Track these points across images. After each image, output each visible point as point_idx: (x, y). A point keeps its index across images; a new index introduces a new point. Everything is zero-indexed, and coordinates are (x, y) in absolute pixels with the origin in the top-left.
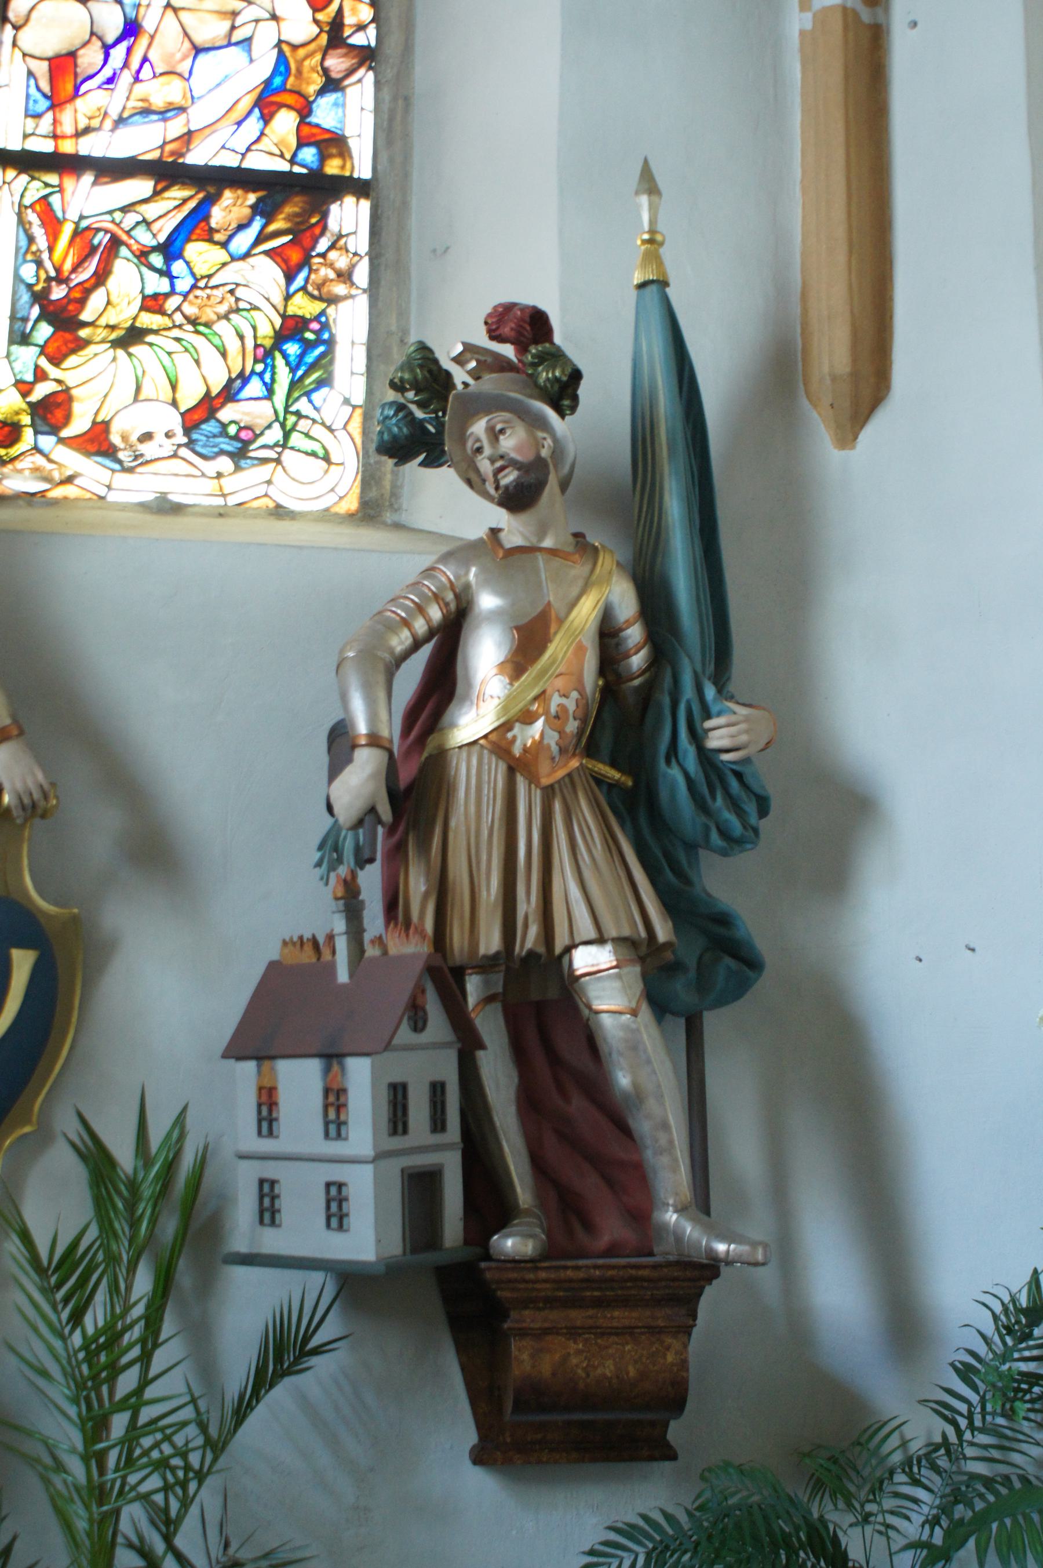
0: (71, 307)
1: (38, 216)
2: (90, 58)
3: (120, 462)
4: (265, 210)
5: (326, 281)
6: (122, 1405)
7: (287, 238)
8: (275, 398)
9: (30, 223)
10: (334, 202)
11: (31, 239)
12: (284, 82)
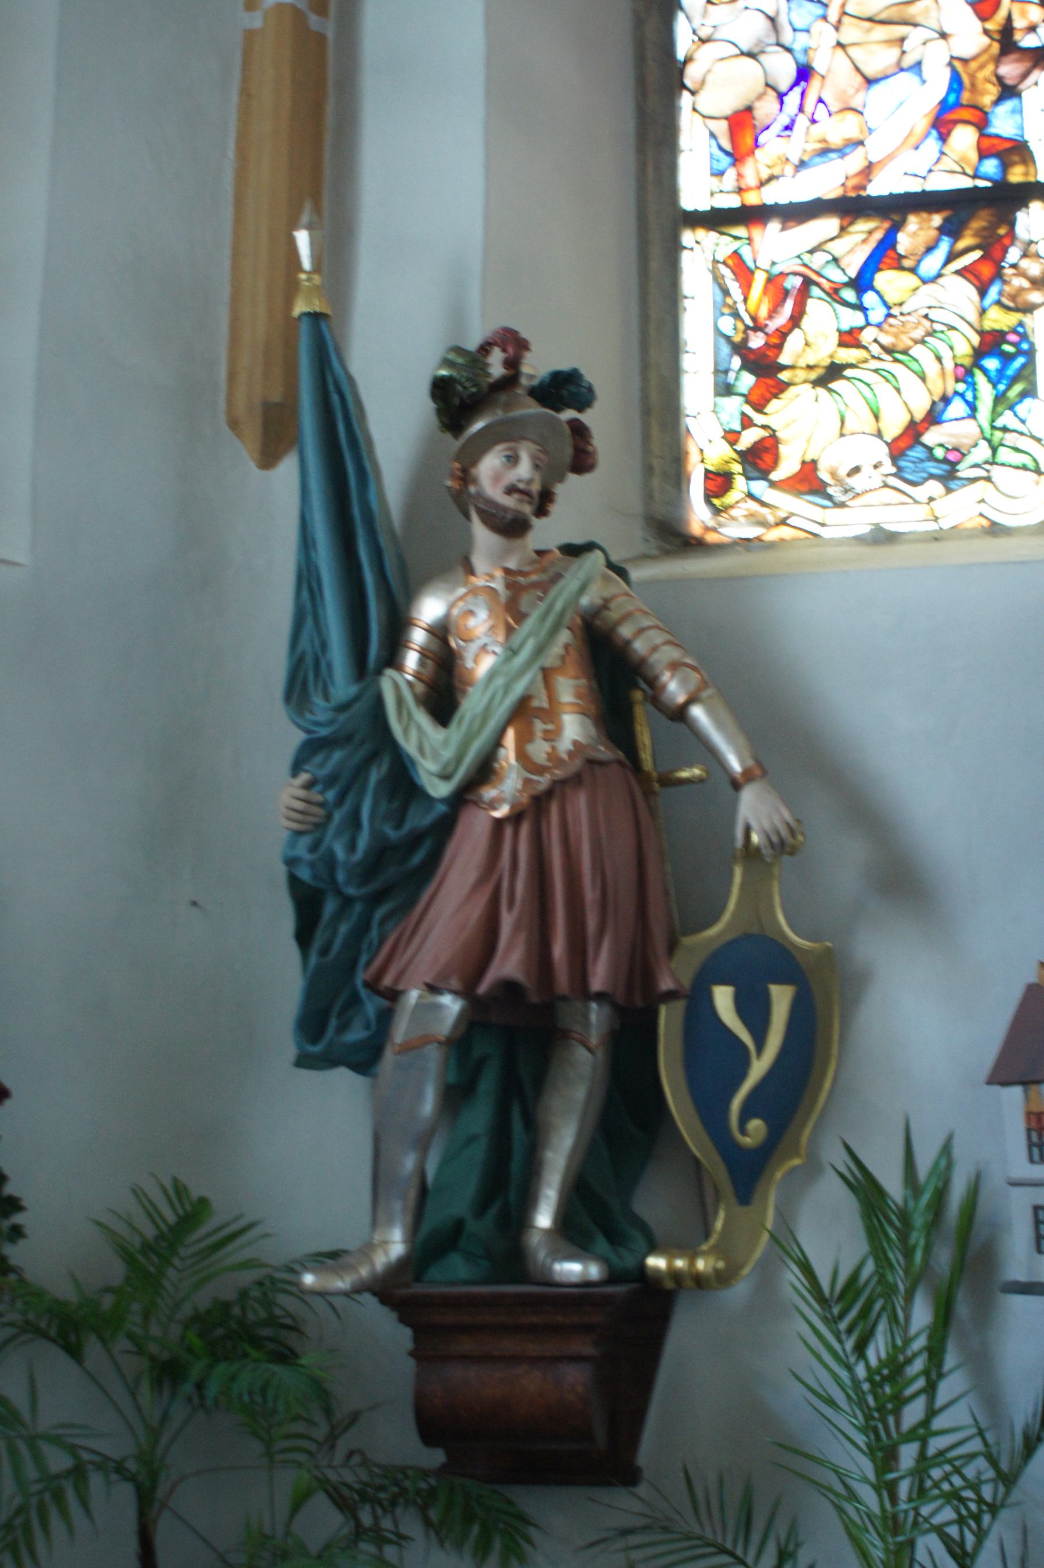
0: (770, 354)
1: (732, 271)
2: (766, 108)
3: (829, 497)
4: (952, 230)
5: (1021, 290)
6: (911, 1435)
7: (977, 254)
8: (978, 415)
9: (723, 276)
10: (1019, 209)
11: (726, 292)
12: (958, 98)
